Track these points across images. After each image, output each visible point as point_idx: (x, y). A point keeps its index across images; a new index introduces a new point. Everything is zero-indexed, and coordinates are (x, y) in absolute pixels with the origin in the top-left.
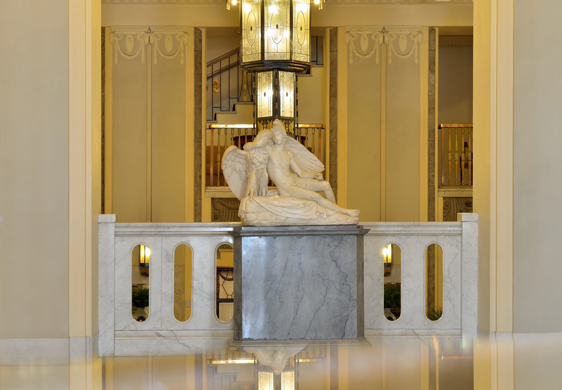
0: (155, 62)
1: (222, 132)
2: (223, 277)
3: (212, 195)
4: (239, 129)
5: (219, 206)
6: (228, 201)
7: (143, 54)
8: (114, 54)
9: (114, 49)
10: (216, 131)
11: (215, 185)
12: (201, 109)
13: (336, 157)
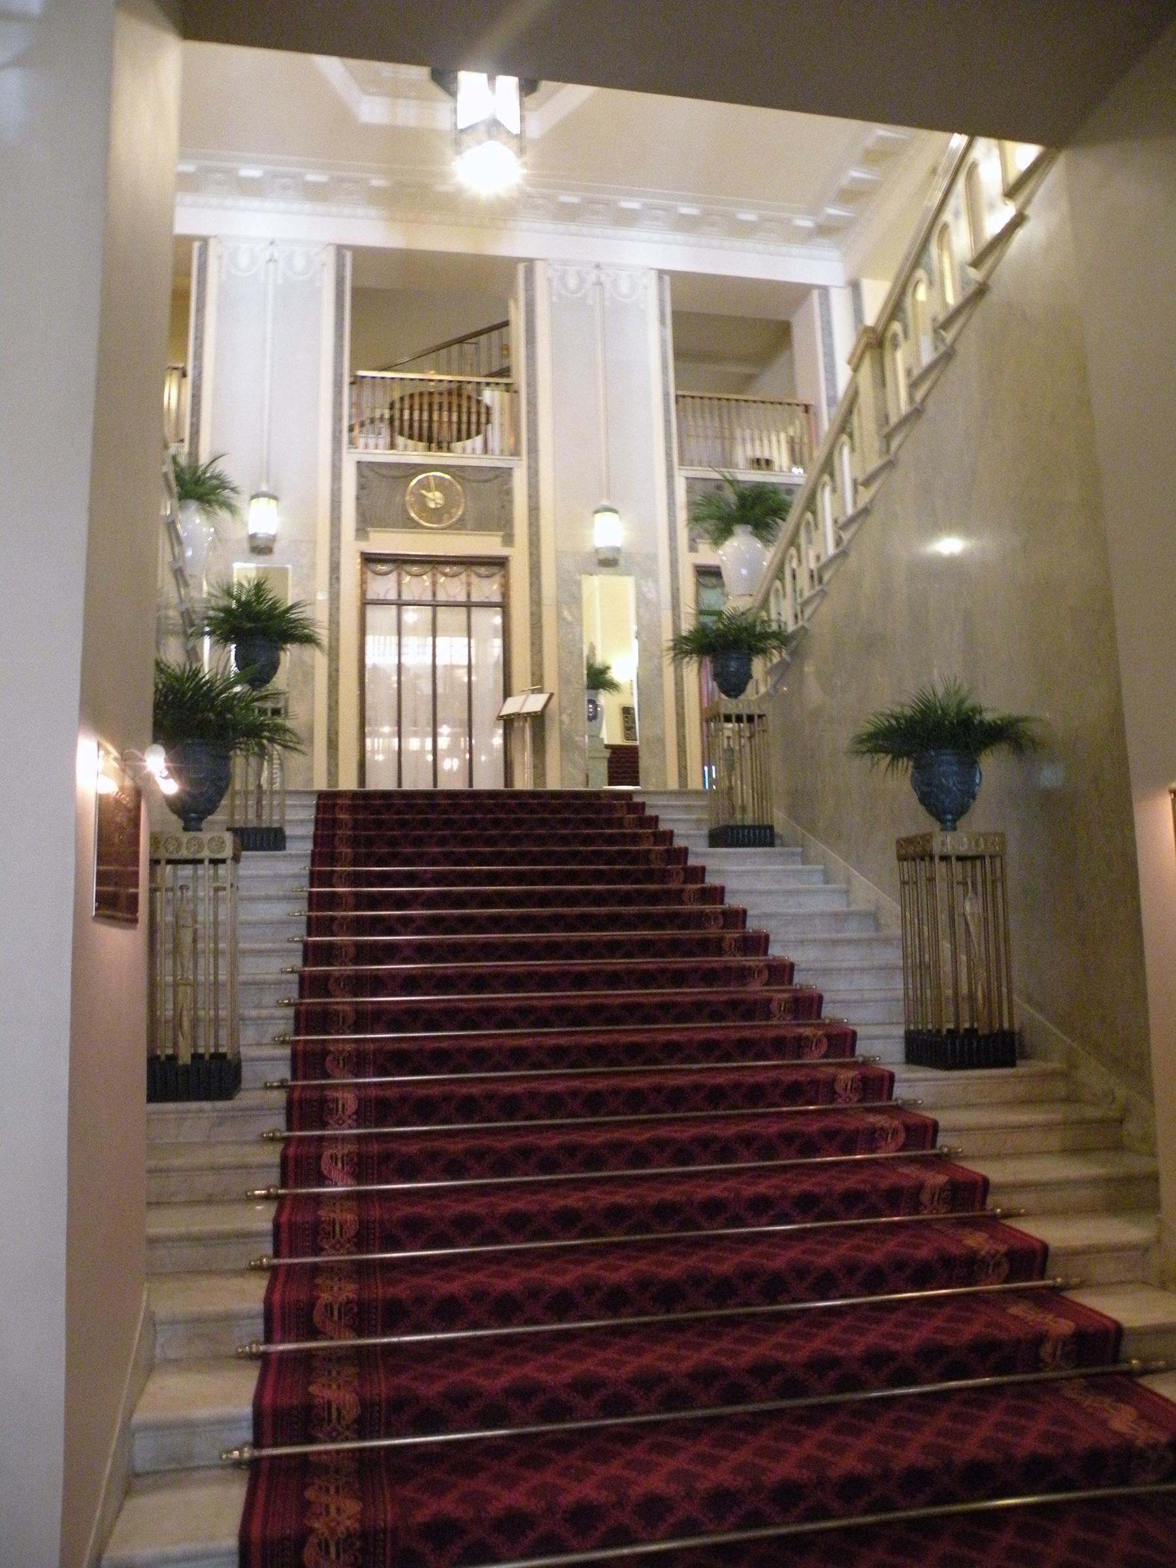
5: (367, 473)
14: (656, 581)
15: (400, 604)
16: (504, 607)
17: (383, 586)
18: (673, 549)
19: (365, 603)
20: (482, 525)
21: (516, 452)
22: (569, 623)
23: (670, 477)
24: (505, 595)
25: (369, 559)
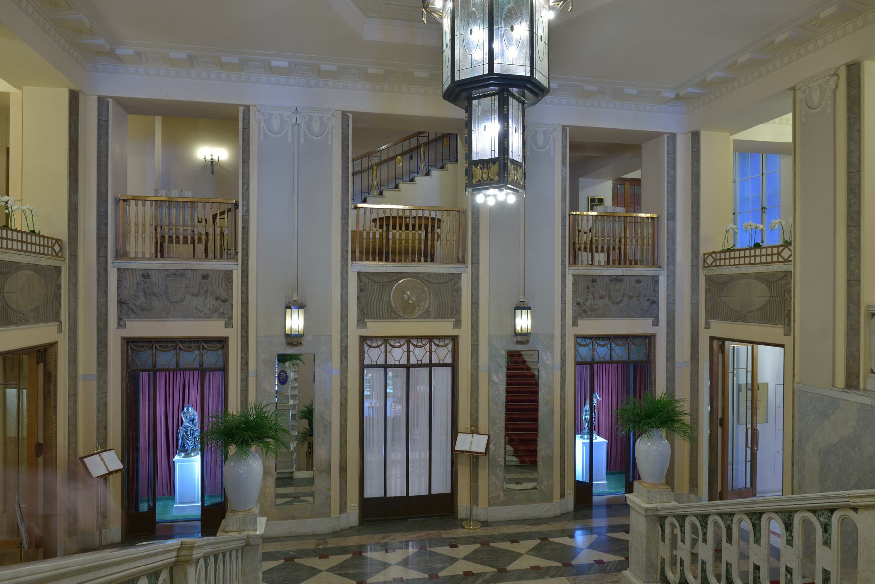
0: (302, 141)
1: (368, 212)
2: (368, 345)
3: (358, 269)
4: (384, 209)
5: (364, 279)
7: (290, 133)
8: (259, 132)
9: (259, 127)
10: (361, 211)
11: (361, 260)
12: (347, 188)
13: (478, 237)
14: (552, 352)
15: (386, 366)
16: (454, 366)
17: (374, 355)
18: (563, 327)
19: (363, 367)
20: (440, 315)
21: (462, 261)
22: (496, 384)
23: (564, 276)
24: (576, 350)
25: (363, 339)
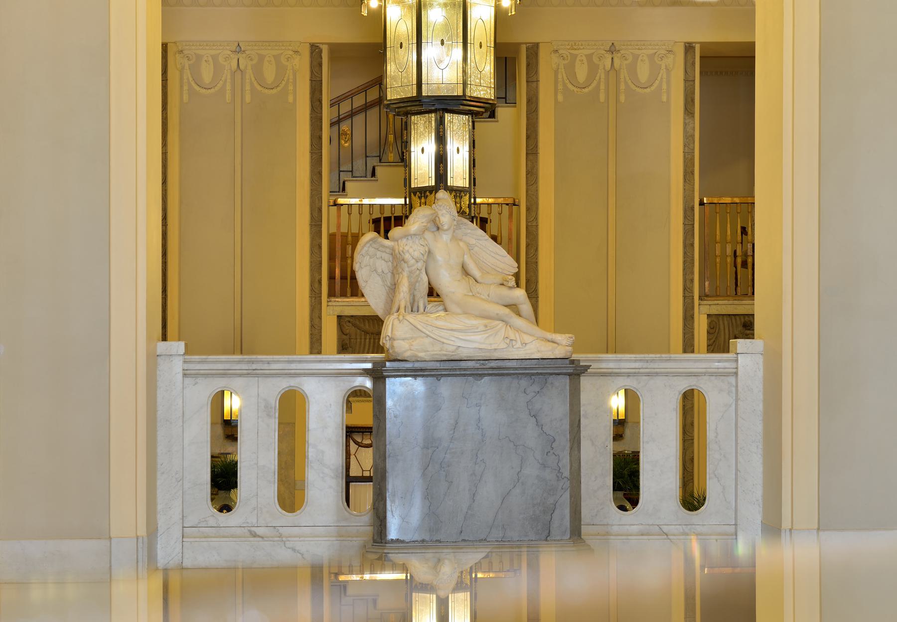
0: (248, 98)
1: (355, 210)
2: (356, 443)
3: (339, 311)
4: (382, 206)
5: (349, 328)
6: (364, 321)
7: (228, 87)
8: (181, 87)
9: (181, 79)
10: (344, 210)
11: (343, 294)
12: (320, 173)
13: (537, 250)
